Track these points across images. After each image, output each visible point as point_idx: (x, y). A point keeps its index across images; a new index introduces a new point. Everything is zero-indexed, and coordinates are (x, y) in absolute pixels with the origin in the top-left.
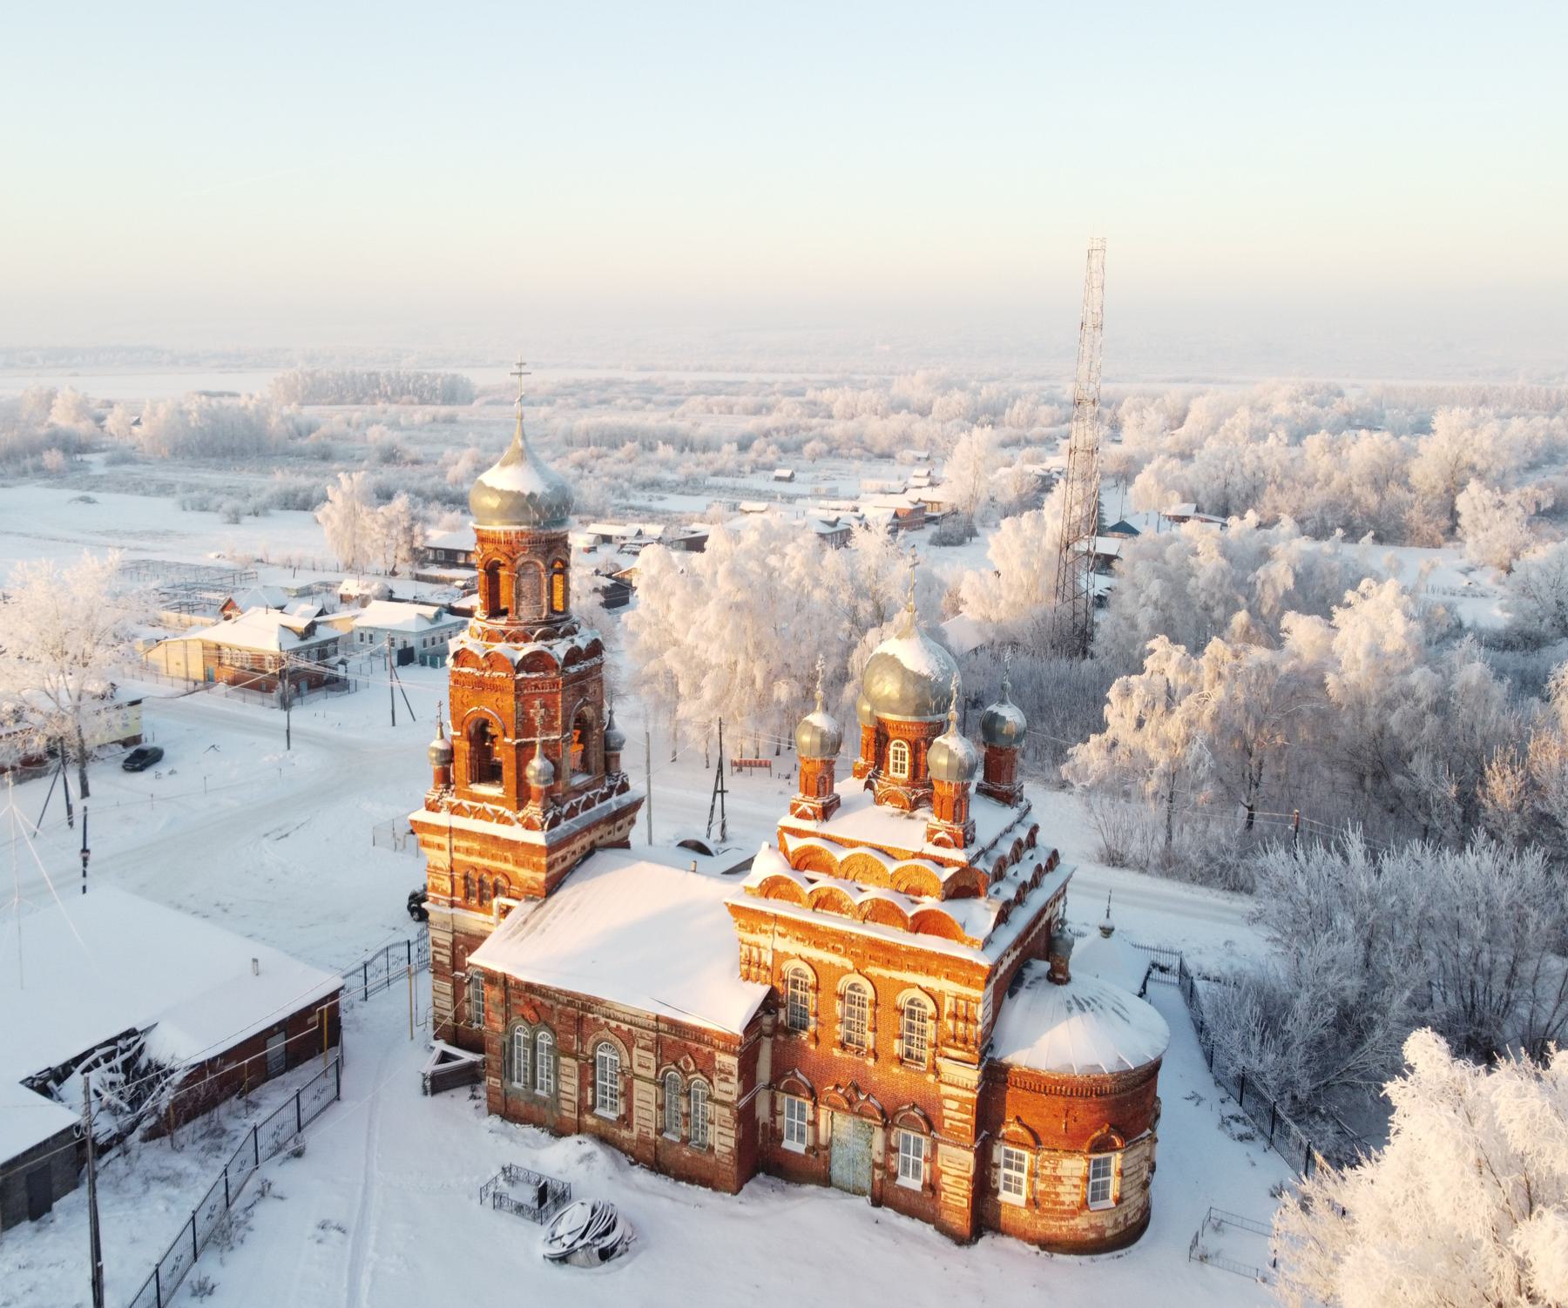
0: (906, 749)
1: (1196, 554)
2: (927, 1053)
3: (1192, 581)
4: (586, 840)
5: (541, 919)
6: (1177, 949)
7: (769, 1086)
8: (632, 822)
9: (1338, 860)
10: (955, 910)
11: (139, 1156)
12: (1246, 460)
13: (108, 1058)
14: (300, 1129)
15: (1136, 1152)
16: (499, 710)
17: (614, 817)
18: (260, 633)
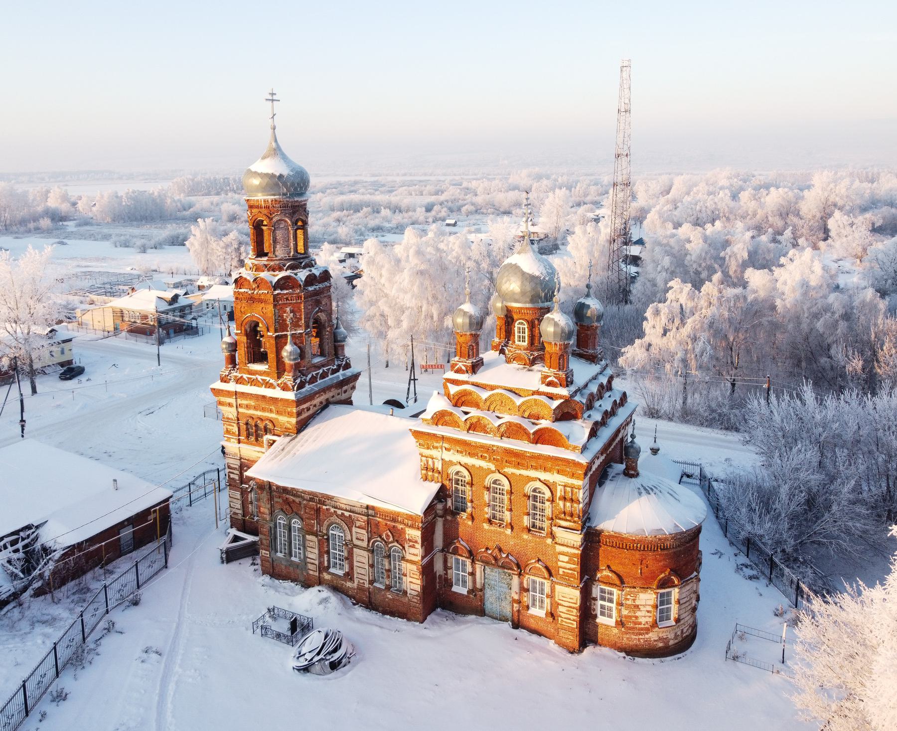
0: (526, 326)
1: (689, 241)
2: (546, 524)
3: (688, 257)
4: (323, 398)
5: (293, 447)
6: (698, 462)
7: (442, 550)
8: (354, 388)
9: (798, 402)
10: (562, 428)
11: (29, 607)
12: (708, 204)
13: (14, 543)
14: (138, 587)
15: (688, 588)
16: (264, 315)
17: (341, 384)
18: (145, 302)
